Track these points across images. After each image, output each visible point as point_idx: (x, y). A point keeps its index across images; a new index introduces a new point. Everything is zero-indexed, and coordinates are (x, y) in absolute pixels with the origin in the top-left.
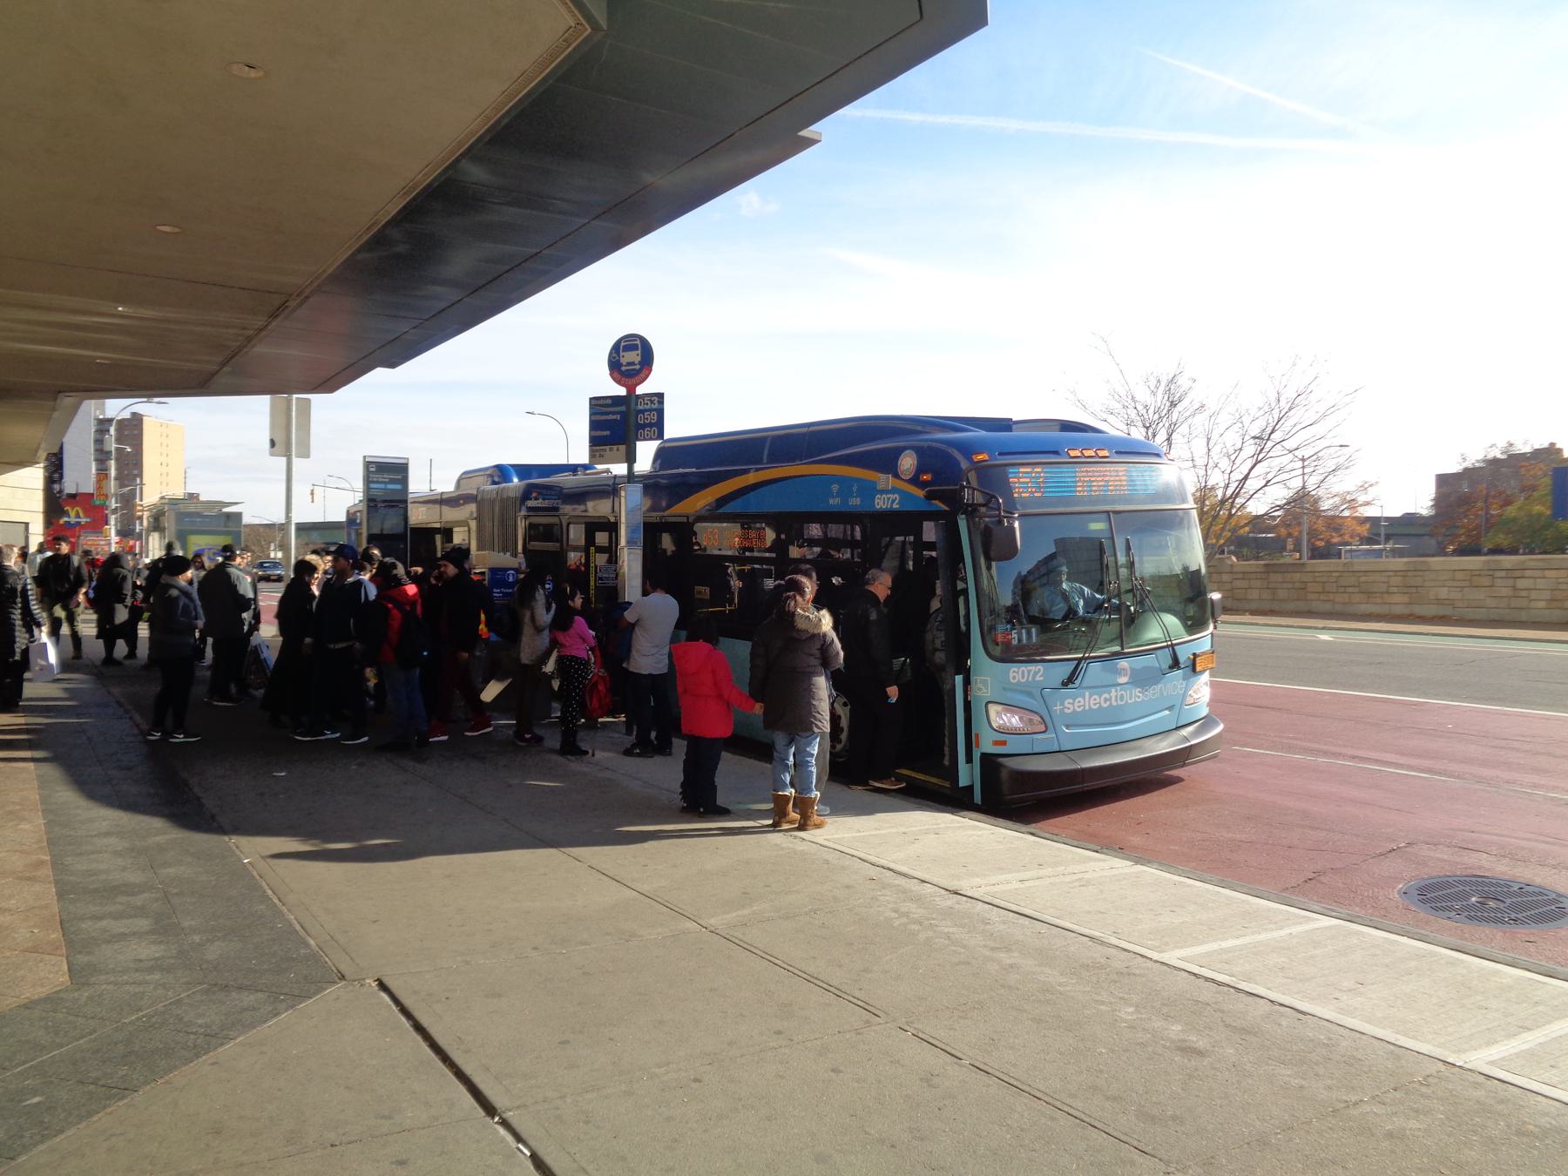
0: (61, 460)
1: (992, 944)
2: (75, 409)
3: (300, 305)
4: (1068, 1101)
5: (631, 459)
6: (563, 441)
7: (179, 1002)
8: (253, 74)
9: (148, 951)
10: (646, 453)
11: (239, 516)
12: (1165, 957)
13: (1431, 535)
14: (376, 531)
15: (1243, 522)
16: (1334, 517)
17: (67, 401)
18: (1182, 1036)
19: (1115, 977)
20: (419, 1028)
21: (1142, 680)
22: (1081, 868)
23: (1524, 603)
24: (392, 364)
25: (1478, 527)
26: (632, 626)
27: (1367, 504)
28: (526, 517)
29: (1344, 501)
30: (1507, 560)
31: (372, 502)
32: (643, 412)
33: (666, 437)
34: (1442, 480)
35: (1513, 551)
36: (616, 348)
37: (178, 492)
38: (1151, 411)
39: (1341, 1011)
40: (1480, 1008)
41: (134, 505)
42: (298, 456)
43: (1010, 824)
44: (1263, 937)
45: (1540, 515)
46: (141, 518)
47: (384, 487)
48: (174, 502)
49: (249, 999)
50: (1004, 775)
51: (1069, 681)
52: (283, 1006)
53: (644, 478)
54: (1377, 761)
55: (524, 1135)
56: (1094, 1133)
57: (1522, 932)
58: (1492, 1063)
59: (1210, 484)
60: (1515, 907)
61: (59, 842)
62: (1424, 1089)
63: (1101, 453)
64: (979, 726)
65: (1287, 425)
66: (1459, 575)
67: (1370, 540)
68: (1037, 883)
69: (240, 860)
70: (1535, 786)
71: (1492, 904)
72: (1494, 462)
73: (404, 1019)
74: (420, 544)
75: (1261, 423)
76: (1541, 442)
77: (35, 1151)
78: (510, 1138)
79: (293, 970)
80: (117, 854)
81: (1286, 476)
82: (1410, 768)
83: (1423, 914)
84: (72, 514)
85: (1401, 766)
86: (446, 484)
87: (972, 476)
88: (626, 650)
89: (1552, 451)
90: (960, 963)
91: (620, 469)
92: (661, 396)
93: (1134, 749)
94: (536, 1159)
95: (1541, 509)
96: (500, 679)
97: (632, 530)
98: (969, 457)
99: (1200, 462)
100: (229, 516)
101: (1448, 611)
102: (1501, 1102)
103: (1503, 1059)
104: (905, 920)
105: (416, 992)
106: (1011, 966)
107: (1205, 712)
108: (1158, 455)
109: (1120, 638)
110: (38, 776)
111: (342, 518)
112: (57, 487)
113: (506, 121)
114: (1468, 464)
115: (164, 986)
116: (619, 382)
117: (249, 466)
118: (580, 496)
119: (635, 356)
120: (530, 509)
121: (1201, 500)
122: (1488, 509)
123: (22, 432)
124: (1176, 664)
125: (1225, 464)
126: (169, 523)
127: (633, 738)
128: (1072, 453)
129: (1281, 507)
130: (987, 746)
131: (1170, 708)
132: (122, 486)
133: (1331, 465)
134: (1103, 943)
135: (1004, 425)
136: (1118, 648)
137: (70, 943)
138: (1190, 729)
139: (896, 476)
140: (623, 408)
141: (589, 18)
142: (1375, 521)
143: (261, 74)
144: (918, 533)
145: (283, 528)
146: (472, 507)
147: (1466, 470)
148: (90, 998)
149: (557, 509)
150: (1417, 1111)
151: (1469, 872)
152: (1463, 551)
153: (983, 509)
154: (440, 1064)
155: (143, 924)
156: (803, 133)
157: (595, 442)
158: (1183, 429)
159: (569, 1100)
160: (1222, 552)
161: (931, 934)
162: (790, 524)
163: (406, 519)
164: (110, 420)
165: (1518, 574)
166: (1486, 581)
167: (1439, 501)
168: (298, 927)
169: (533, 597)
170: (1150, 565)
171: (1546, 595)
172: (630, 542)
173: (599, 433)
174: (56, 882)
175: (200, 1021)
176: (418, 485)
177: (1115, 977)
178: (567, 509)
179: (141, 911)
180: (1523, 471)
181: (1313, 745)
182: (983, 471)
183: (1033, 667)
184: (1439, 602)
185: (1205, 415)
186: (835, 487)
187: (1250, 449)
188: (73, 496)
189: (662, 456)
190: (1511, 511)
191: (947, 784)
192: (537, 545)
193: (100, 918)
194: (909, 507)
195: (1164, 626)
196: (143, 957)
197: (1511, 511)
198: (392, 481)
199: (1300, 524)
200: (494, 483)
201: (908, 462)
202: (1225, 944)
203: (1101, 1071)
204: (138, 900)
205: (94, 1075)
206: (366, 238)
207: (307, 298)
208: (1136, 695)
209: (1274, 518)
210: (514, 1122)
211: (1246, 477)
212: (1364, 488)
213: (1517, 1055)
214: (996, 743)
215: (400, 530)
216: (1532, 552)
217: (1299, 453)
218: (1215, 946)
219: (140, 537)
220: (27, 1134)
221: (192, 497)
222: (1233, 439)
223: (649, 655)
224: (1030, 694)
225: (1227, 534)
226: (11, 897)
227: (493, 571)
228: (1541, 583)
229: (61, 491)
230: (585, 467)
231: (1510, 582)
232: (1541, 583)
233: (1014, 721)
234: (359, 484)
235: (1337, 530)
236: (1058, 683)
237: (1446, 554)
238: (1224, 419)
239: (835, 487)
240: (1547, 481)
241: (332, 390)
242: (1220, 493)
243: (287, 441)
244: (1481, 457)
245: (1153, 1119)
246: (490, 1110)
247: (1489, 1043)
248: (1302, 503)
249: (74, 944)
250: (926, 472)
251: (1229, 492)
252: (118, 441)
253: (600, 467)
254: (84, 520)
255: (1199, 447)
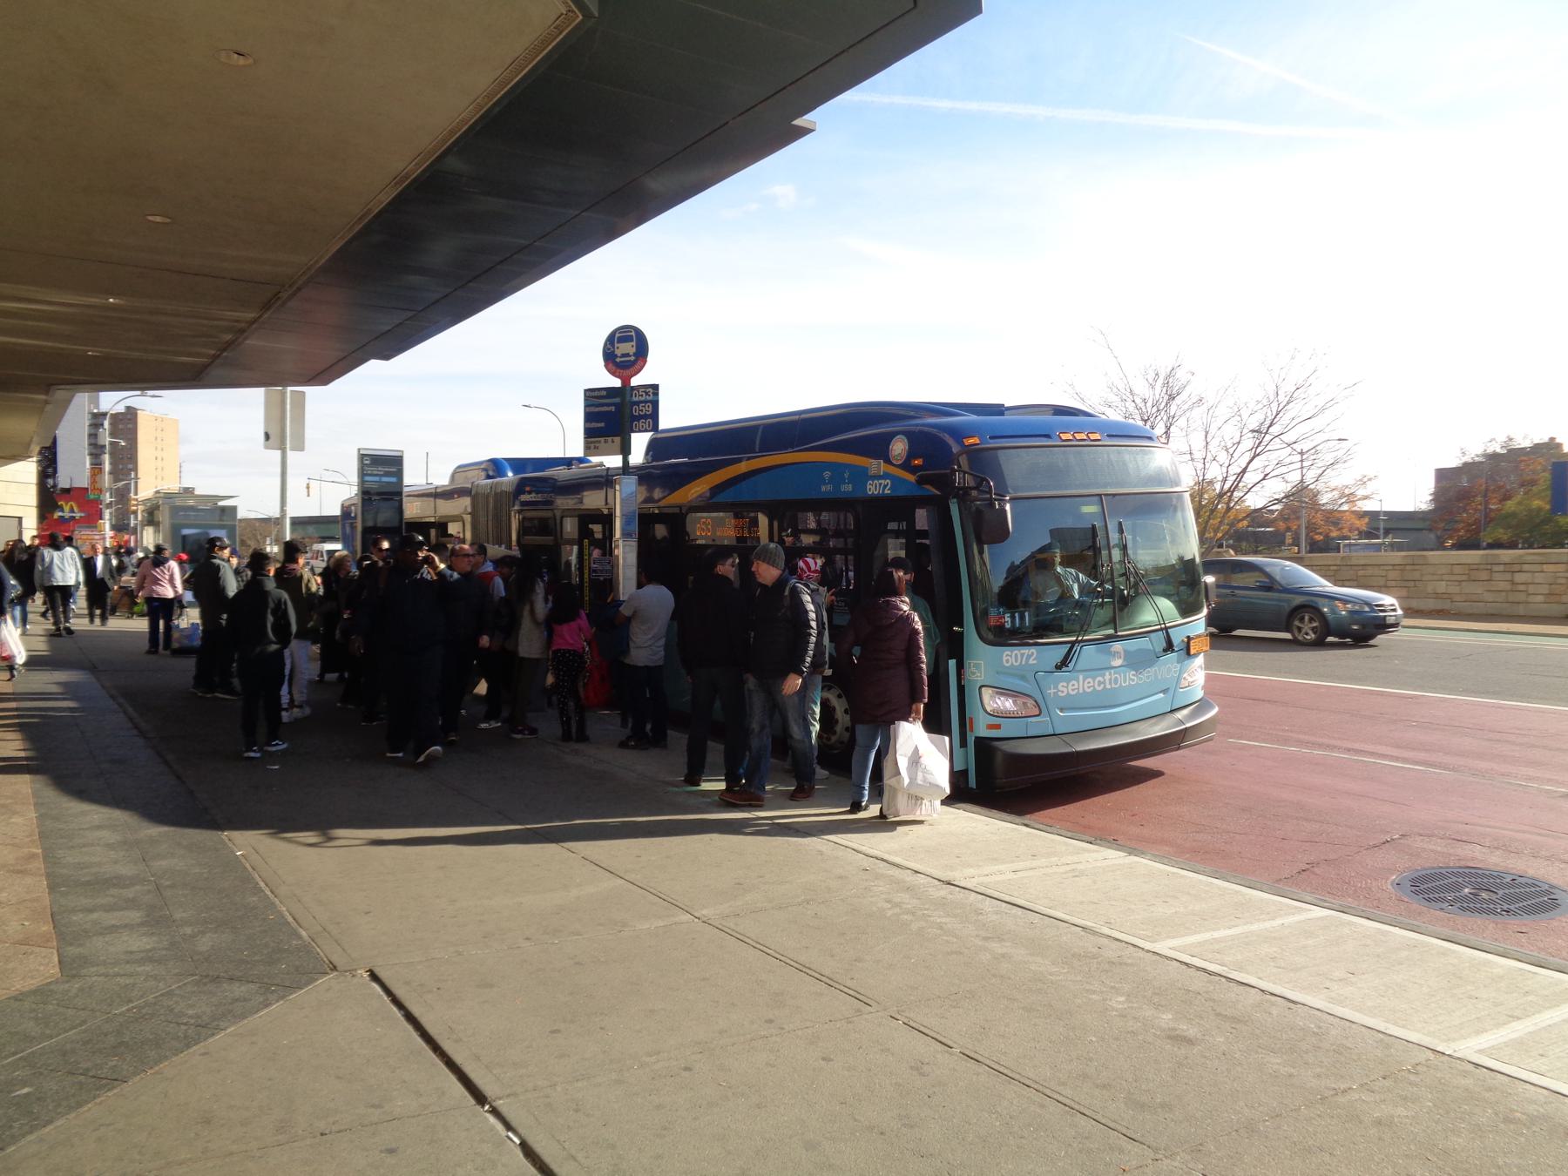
0: (55, 454)
1: (983, 934)
2: (69, 401)
3: (294, 294)
4: (1058, 1089)
5: (625, 450)
6: (558, 435)
7: (170, 994)
8: (242, 61)
9: (139, 943)
10: (640, 443)
11: (234, 509)
12: (1163, 947)
13: (1430, 530)
14: (370, 524)
16: (1332, 512)
17: (60, 394)
18: (1172, 1025)
19: (1107, 966)
20: (410, 1018)
21: (1137, 662)
22: (1075, 858)
23: (1522, 597)
25: (1477, 522)
26: (629, 620)
27: (1366, 498)
28: (520, 512)
29: (1342, 496)
30: (1506, 555)
31: (366, 494)
32: (637, 403)
33: (661, 427)
34: (1442, 475)
35: (1512, 545)
36: (611, 340)
37: (172, 486)
38: (1149, 404)
39: (1331, 1000)
40: (1470, 997)
41: (129, 500)
42: (292, 449)
44: (1254, 927)
45: (1540, 509)
46: (135, 513)
47: (378, 480)
48: (169, 496)
49: (239, 990)
50: (999, 759)
51: (1063, 664)
53: (638, 469)
54: (1372, 754)
55: (514, 1124)
56: (1082, 1121)
57: (1514, 922)
58: (1480, 1051)
59: (1209, 477)
60: (1508, 899)
61: (49, 836)
62: (1412, 1078)
63: (1092, 437)
64: (973, 711)
65: (1285, 419)
66: (1457, 569)
67: (1369, 535)
68: (1031, 873)
69: (233, 853)
70: (1530, 779)
71: (1484, 895)
72: (1494, 457)
74: (409, 534)
75: (1259, 417)
76: (1541, 437)
77: (23, 1142)
78: (500, 1127)
79: (278, 960)
80: (110, 846)
81: (1284, 470)
82: (1405, 760)
83: (1417, 904)
84: (67, 508)
85: (1397, 759)
86: (441, 478)
87: (963, 460)
88: (624, 645)
89: (1552, 446)
90: (952, 953)
91: (614, 461)
92: (655, 387)
93: (1128, 733)
94: (525, 1148)
95: (1540, 503)
97: (627, 521)
98: (960, 442)
99: (1198, 455)
100: (224, 509)
101: (1447, 605)
102: (1490, 1089)
103: (1493, 1047)
104: (897, 910)
105: (407, 983)
106: (1003, 956)
107: (1200, 694)
108: (1150, 438)
109: (1113, 622)
111: (337, 512)
112: (50, 482)
113: (497, 109)
114: (1468, 459)
115: (155, 978)
116: (613, 374)
117: (251, 457)
118: (576, 487)
120: (523, 504)
121: (1197, 495)
122: (1487, 503)
123: (22, 426)
124: (1169, 647)
125: (1223, 457)
126: (164, 517)
127: (628, 731)
128: (1064, 437)
129: (1279, 501)
131: (1164, 691)
132: (116, 480)
133: (1329, 458)
134: (1095, 933)
135: (998, 410)
136: (1111, 631)
138: (1185, 712)
139: (888, 461)
140: (617, 400)
141: (582, 7)
142: (1374, 515)
143: (251, 61)
144: (911, 521)
145: (278, 522)
146: (466, 502)
147: (1466, 464)
148: (81, 990)
149: (550, 502)
150: (1405, 1099)
151: (1463, 863)
152: (1461, 546)
153: (974, 493)
155: (135, 916)
156: (796, 122)
157: (590, 434)
158: (1182, 422)
159: (559, 1089)
160: (1221, 546)
161: (923, 924)
162: (785, 513)
163: (400, 511)
164: (104, 415)
165: (1516, 568)
166: (1484, 575)
167: (1438, 496)
168: (290, 919)
169: (532, 590)
170: (1145, 557)
171: (1545, 589)
172: (626, 534)
173: (594, 425)
174: (48, 876)
175: (190, 1012)
176: (413, 478)
177: (1107, 966)
178: (564, 502)
179: (132, 904)
180: (1522, 466)
181: (1312, 739)
182: (975, 454)
183: (1026, 651)
184: (1437, 596)
185: (1204, 408)
186: (827, 474)
187: (1248, 443)
188: (67, 491)
189: (654, 448)
190: (1510, 505)
192: (530, 539)
193: (91, 911)
194: (901, 492)
195: (1159, 610)
196: (134, 948)
197: (1510, 505)
198: (387, 474)
199: (1298, 518)
200: (489, 477)
201: (899, 447)
202: (1216, 935)
203: (1091, 1060)
204: (129, 893)
205: (84, 1065)
206: (357, 228)
207: (299, 289)
208: (1130, 678)
209: (1272, 512)
210: (504, 1111)
211: (1244, 471)
212: (1363, 482)
213: (1506, 1044)
214: (991, 727)
215: (396, 524)
216: (1531, 547)
217: (1298, 447)
218: (1207, 936)
219: (134, 531)
220: (16, 1125)
221: (188, 491)
222: (1231, 432)
223: (646, 647)
224: (1023, 678)
225: (1224, 528)
228: (1539, 578)
229: (55, 486)
230: (580, 460)
231: (1508, 576)
232: (1539, 578)
233: (1008, 704)
234: (354, 478)
235: (1335, 524)
236: (1051, 667)
237: (1445, 549)
238: (1223, 412)
239: (827, 474)
240: (1547, 475)
241: (326, 382)
242: (1218, 487)
243: (281, 434)
244: (1480, 452)
245: (1142, 1106)
246: (481, 1099)
247: (1478, 1032)
248: (1300, 498)
249: (64, 934)
250: (916, 458)
251: (1227, 486)
252: (112, 434)
253: (595, 460)
254: (78, 515)
255: (1197, 442)
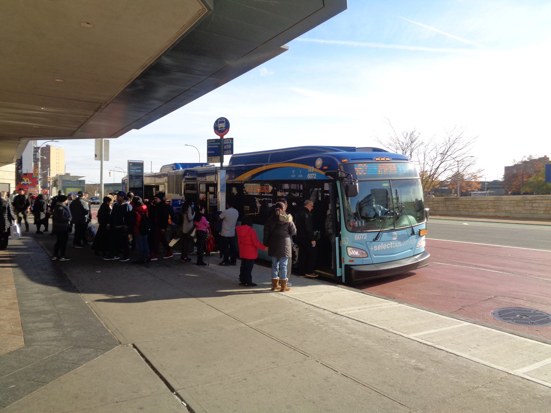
0: (21, 162)
1: (348, 332)
2: (26, 144)
3: (106, 107)
4: (375, 387)
5: (222, 161)
6: (198, 155)
7: (63, 352)
8: (89, 26)
9: (52, 334)
10: (227, 159)
11: (84, 181)
12: (410, 336)
13: (503, 188)
14: (132, 186)
15: (437, 183)
16: (469, 182)
17: (23, 141)
18: (415, 364)
19: (392, 343)
20: (147, 361)
21: (401, 239)
22: (380, 305)
23: (535, 212)
24: (138, 128)
25: (519, 185)
26: (222, 220)
27: (480, 177)
28: (185, 182)
29: (472, 176)
30: (529, 197)
31: (131, 176)
32: (226, 145)
33: (234, 153)
34: (507, 169)
35: (532, 194)
36: (217, 122)
37: (62, 173)
38: (404, 144)
39: (471, 355)
40: (520, 354)
41: (47, 178)
42: (105, 160)
43: (355, 289)
44: (444, 329)
45: (541, 181)
46: (49, 182)
47: (135, 171)
48: (61, 176)
49: (88, 351)
51: (376, 239)
52: (100, 353)
53: (226, 168)
54: (484, 267)
55: (184, 399)
56: (385, 398)
57: (535, 327)
58: (524, 373)
59: (425, 170)
60: (532, 319)
61: (21, 296)
62: (500, 383)
63: (387, 159)
64: (344, 255)
65: (452, 149)
66: (513, 202)
67: (481, 190)
68: (364, 310)
69: (84, 302)
70: (539, 276)
71: (524, 317)
72: (525, 162)
73: (142, 358)
74: (148, 191)
75: (443, 149)
76: (542, 155)
77: (12, 404)
78: (179, 400)
79: (103, 341)
80: (41, 300)
81: (452, 167)
82: (496, 270)
83: (500, 321)
84: (25, 180)
85: (492, 269)
86: (157, 170)
87: (342, 167)
88: (220, 228)
89: (545, 158)
90: (337, 338)
91: (218, 165)
92: (232, 139)
93: (398, 263)
94: (188, 407)
95: (542, 179)
96: (176, 239)
97: (222, 186)
98: (340, 161)
99: (422, 162)
100: (80, 181)
101: (509, 215)
102: (528, 387)
103: (528, 372)
104: (318, 323)
105: (146, 349)
106: (355, 339)
107: (423, 250)
108: (407, 160)
109: (394, 224)
110: (13, 273)
111: (120, 182)
112: (20, 171)
113: (178, 42)
114: (516, 163)
115: (58, 346)
116: (217, 134)
117: (87, 164)
118: (204, 174)
119: (223, 125)
120: (186, 179)
121: (422, 176)
122: (523, 179)
123: (8, 152)
124: (413, 233)
125: (430, 163)
126: (59, 184)
127: (222, 259)
128: (377, 159)
129: (450, 178)
130: (347, 262)
131: (411, 249)
132: (43, 171)
133: (468, 163)
134: (388, 331)
135: (353, 149)
136: (393, 228)
137: (24, 331)
138: (418, 256)
139: (315, 167)
140: (219, 143)
141: (207, 6)
142: (483, 183)
143: (92, 26)
144: (323, 187)
145: (99, 185)
146: (166, 178)
147: (515, 165)
148: (32, 350)
149: (196, 179)
150: (498, 390)
151: (516, 306)
152: (514, 194)
153: (345, 179)
154: (155, 374)
155: (50, 324)
156: (282, 47)
157: (209, 155)
158: (416, 151)
159: (200, 386)
160: (430, 194)
161: (327, 328)
162: (277, 184)
163: (143, 182)
164: (39, 148)
165: (533, 201)
166: (522, 204)
167: (506, 176)
168: (105, 326)
169: (187, 210)
170: (404, 198)
171: (543, 209)
172: (221, 190)
173: (211, 152)
174: (20, 310)
175: (70, 359)
176: (147, 170)
177: (392, 343)
178: (199, 179)
179: (49, 320)
180: (535, 165)
181: (461, 262)
182: (345, 165)
183: (363, 234)
184: (506, 211)
185: (424, 146)
186: (293, 171)
187: (439, 158)
188: (26, 174)
189: (232, 160)
190: (531, 179)
191: (333, 276)
192: (189, 191)
193: (35, 322)
194: (320, 178)
195: (409, 220)
196: (50, 336)
197: (531, 179)
198: (138, 169)
199: (457, 184)
200: (174, 170)
201: (319, 162)
202: (430, 332)
203: (387, 376)
204: (49, 316)
205: (33, 377)
206: (128, 83)
207: (108, 104)
208: (399, 244)
209: (448, 182)
210: (181, 394)
211: (438, 168)
212: (479, 171)
213: (533, 371)
214: (350, 261)
215: (141, 186)
216: (538, 194)
217: (456, 159)
218: (427, 332)
219: (49, 188)
220: (10, 398)
221: (68, 175)
222: (433, 154)
223: (228, 230)
224: (362, 244)
225: (431, 188)
226: (4, 315)
227: (173, 200)
228: (541, 205)
229: (21, 173)
230: (206, 164)
231: (531, 204)
232: (541, 205)
233: (356, 253)
234: (126, 170)
235: (470, 186)
236: (372, 240)
237: (508, 195)
238: (430, 147)
239: (293, 171)
240: (544, 169)
241: (117, 137)
242: (429, 173)
243: (101, 155)
244: (520, 160)
245: (405, 393)
246: (172, 390)
247: (523, 366)
248: (457, 177)
249: (26, 331)
250: (325, 166)
251: (432, 173)
252: (42, 155)
253: (211, 164)
254: (29, 183)
255: (421, 157)
